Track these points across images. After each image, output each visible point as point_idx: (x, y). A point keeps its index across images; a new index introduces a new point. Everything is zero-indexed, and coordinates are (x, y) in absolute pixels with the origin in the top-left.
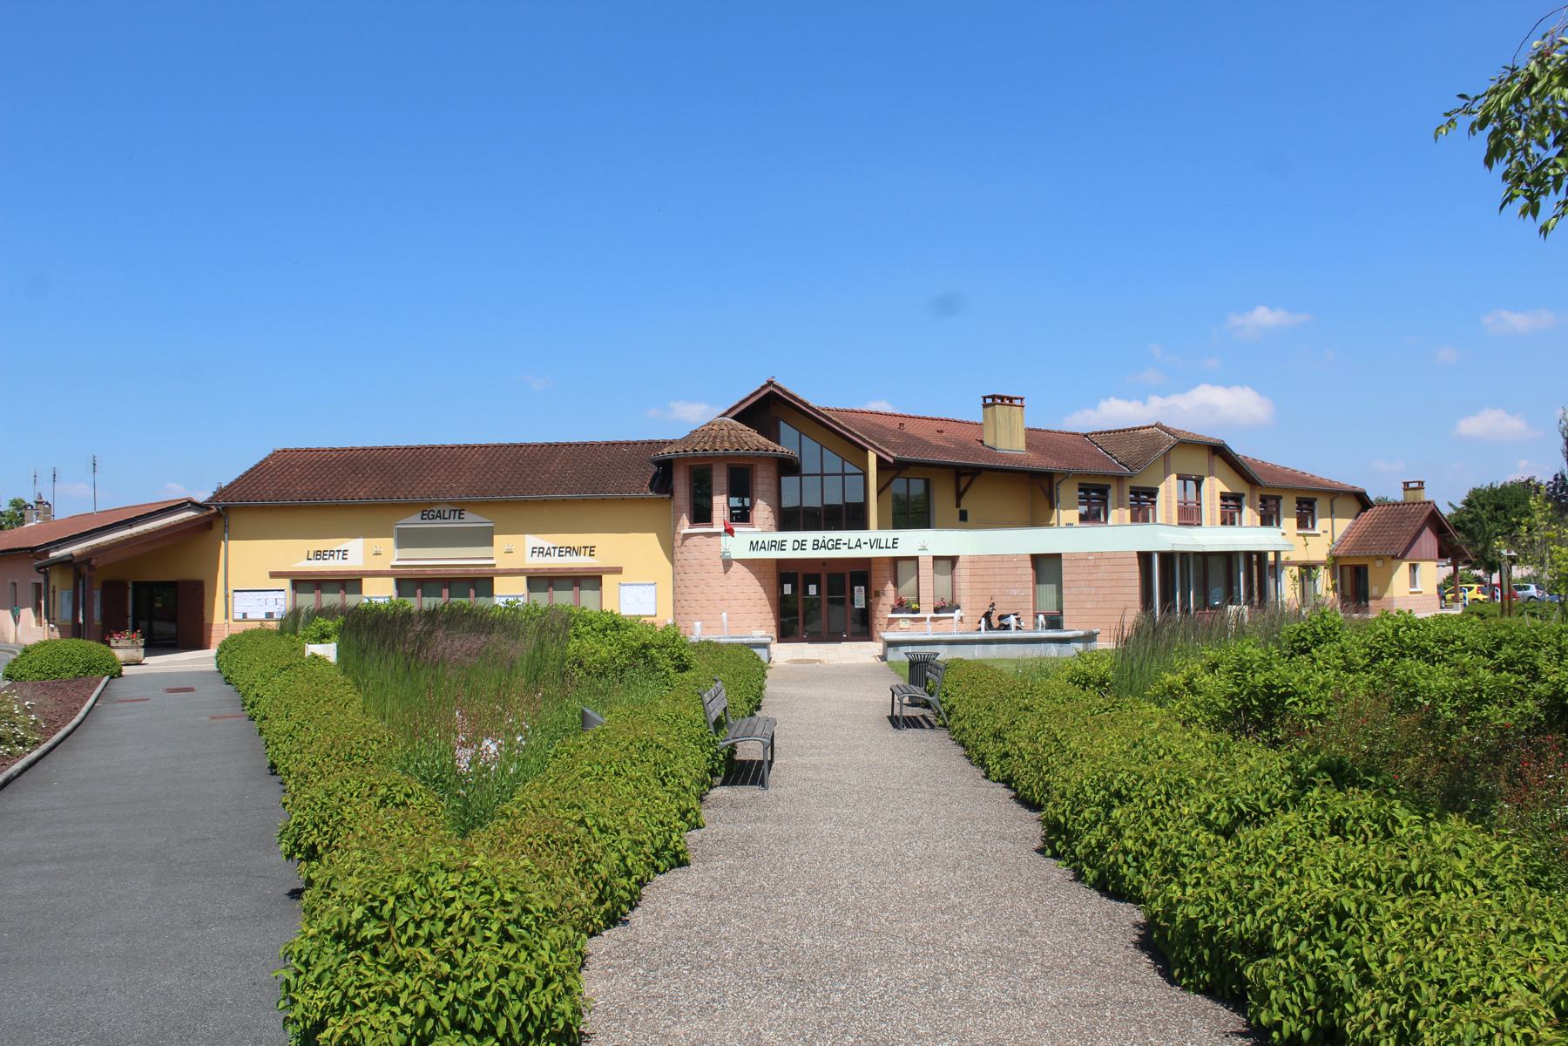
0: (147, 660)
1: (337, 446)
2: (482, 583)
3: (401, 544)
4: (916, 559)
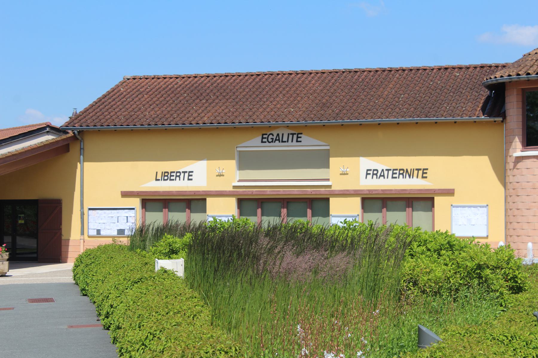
0: (12, 272)
1: (182, 73)
2: (318, 204)
3: (242, 166)
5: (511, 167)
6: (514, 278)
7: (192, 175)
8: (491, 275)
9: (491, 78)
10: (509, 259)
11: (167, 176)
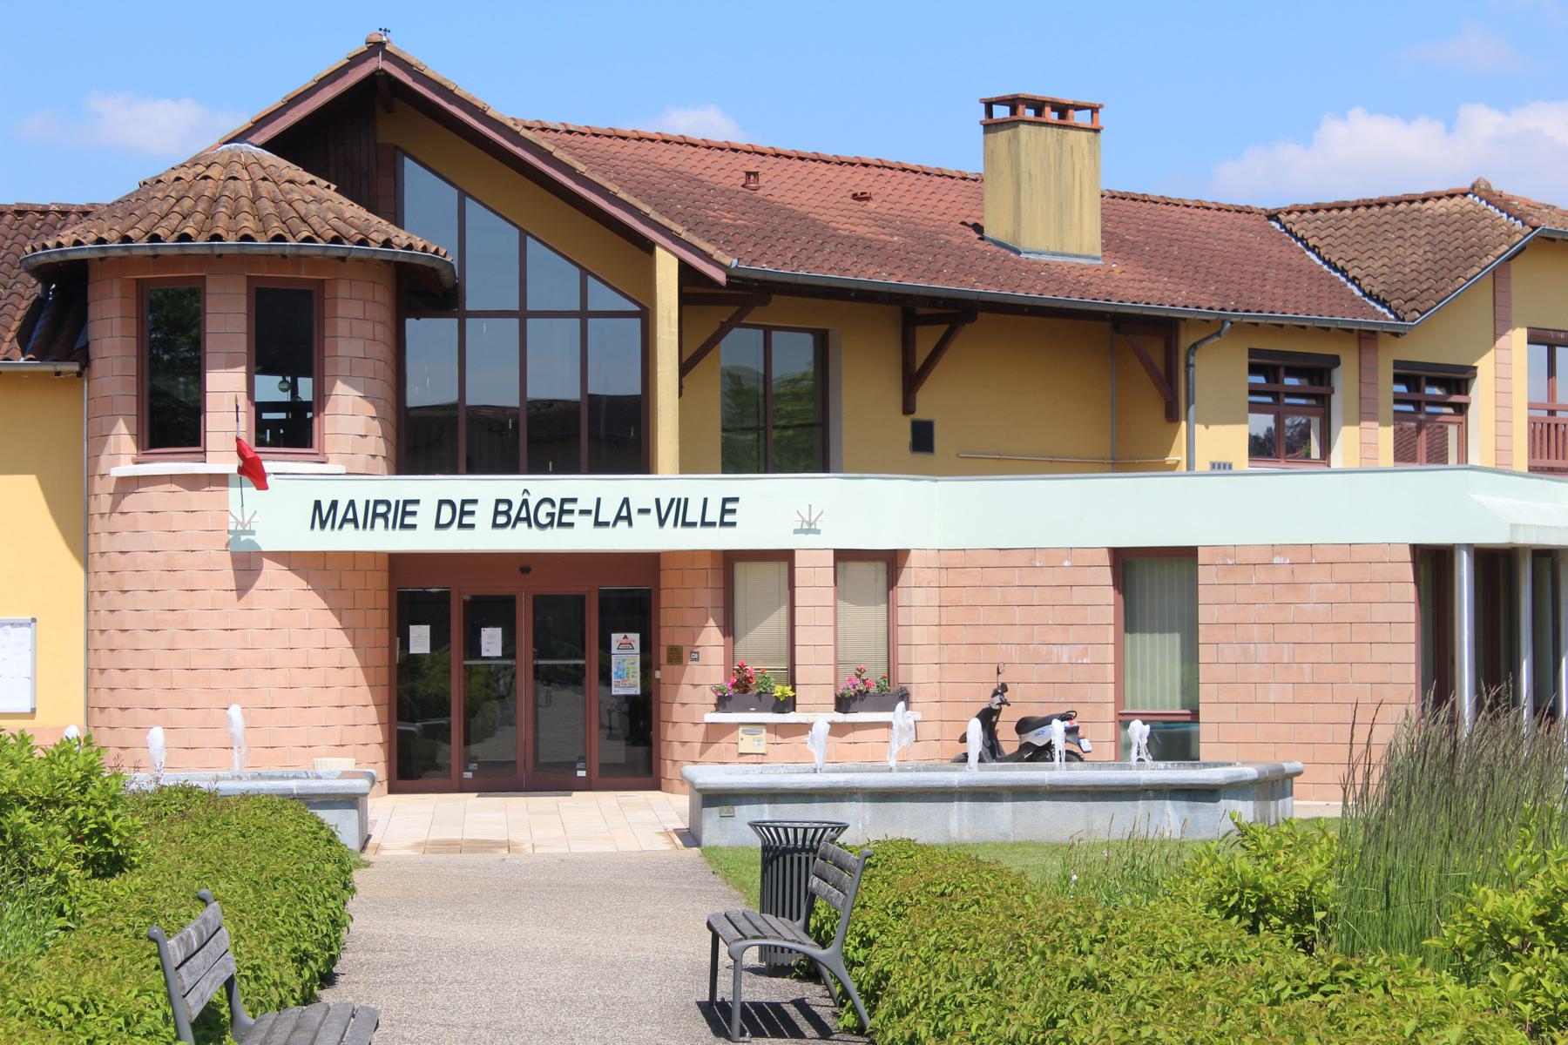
5: (106, 508)
6: (101, 832)
7: (414, 513)
8: (30, 826)
9: (45, 247)
10: (85, 777)
11: (507, 513)
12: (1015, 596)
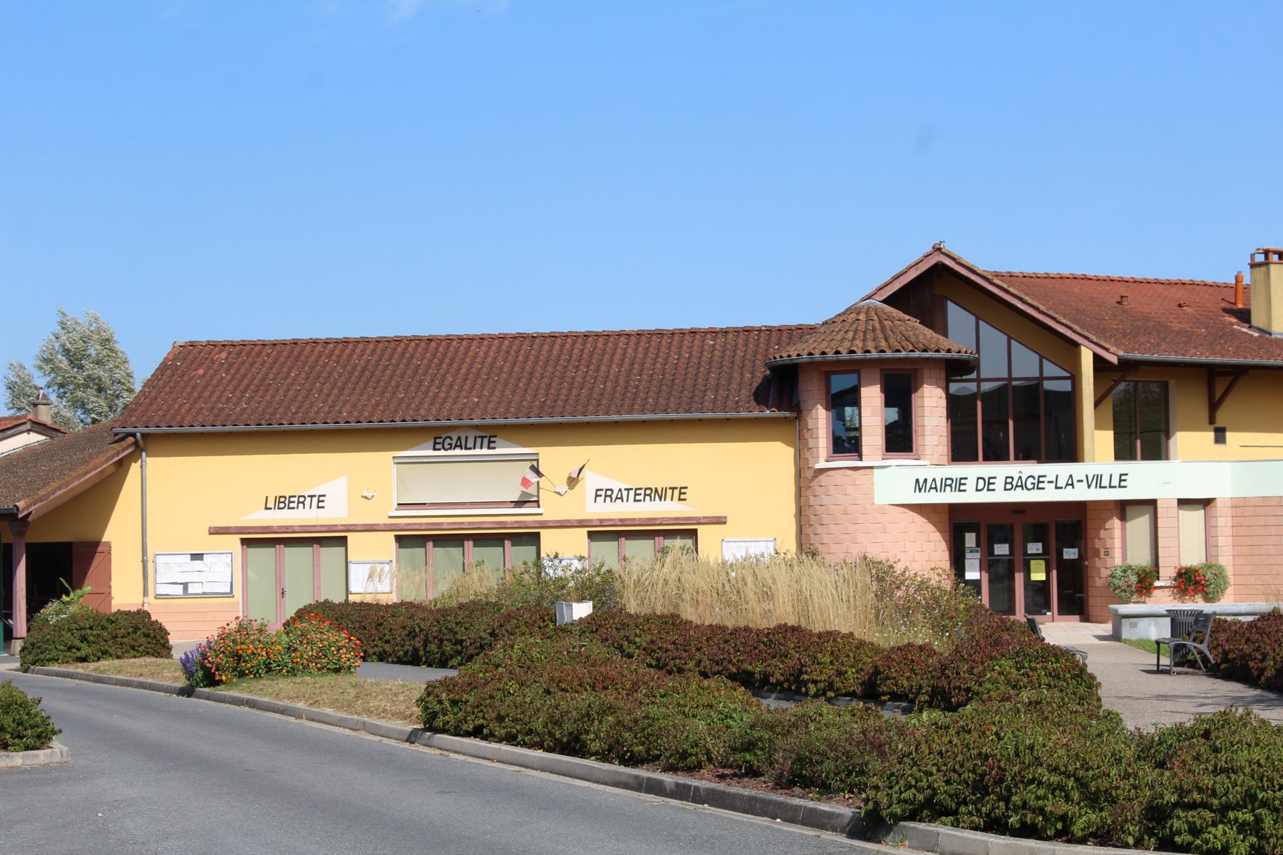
4: (1152, 503)
12: (1271, 520)
